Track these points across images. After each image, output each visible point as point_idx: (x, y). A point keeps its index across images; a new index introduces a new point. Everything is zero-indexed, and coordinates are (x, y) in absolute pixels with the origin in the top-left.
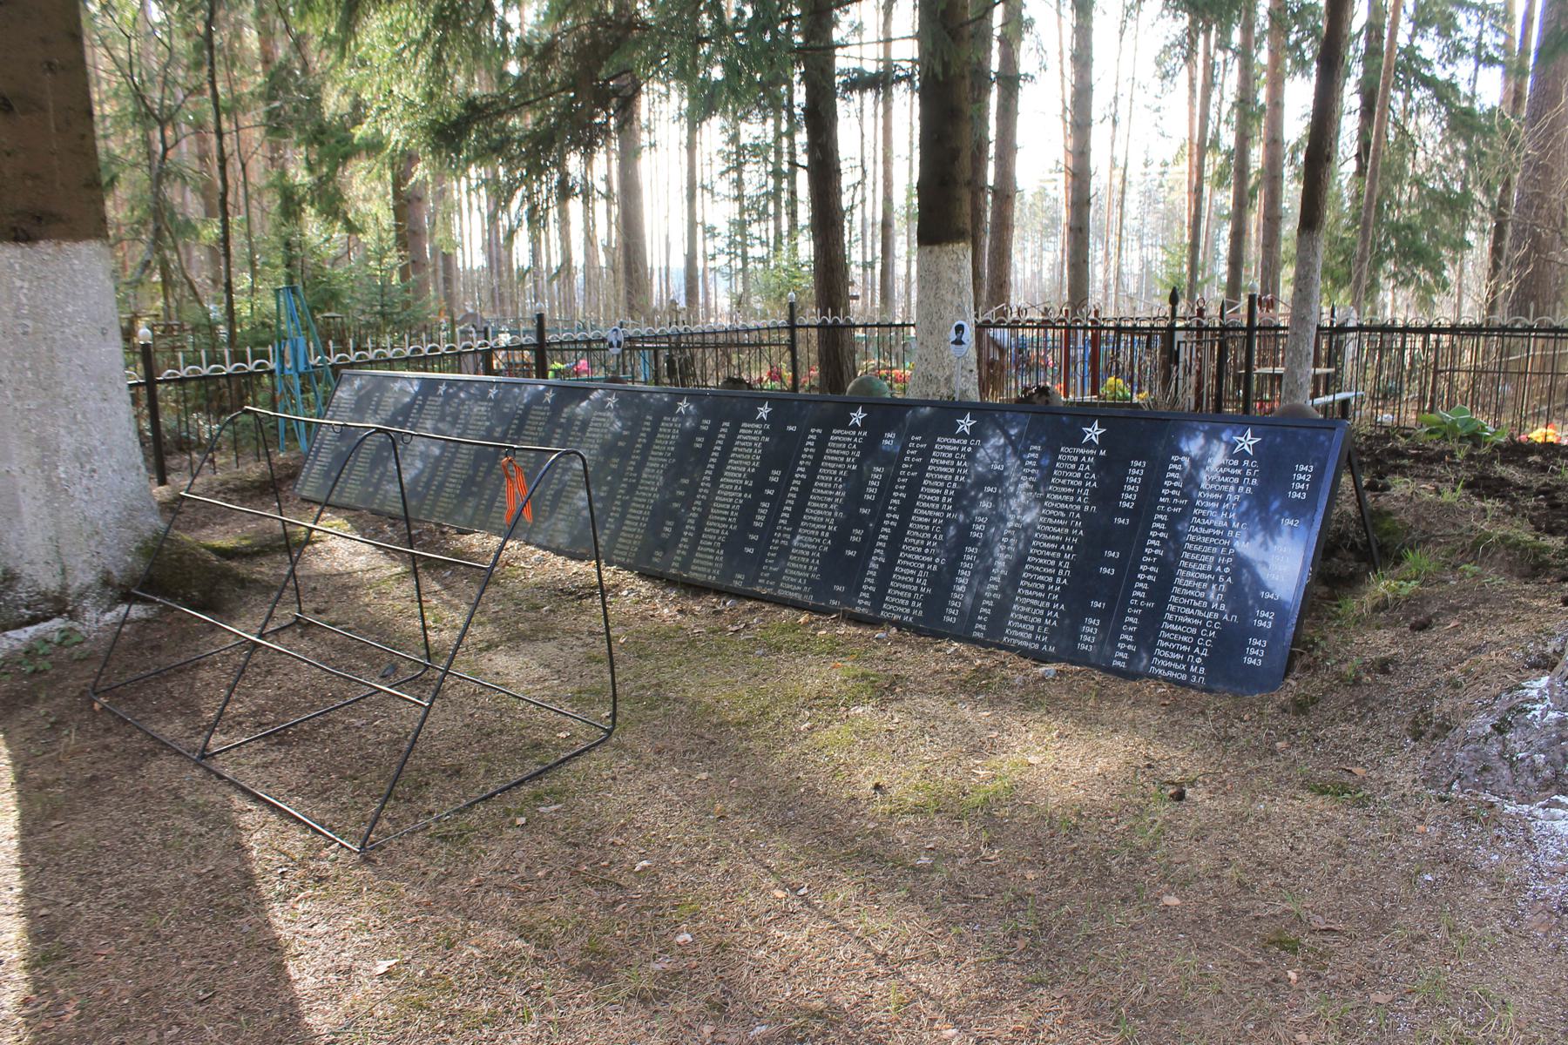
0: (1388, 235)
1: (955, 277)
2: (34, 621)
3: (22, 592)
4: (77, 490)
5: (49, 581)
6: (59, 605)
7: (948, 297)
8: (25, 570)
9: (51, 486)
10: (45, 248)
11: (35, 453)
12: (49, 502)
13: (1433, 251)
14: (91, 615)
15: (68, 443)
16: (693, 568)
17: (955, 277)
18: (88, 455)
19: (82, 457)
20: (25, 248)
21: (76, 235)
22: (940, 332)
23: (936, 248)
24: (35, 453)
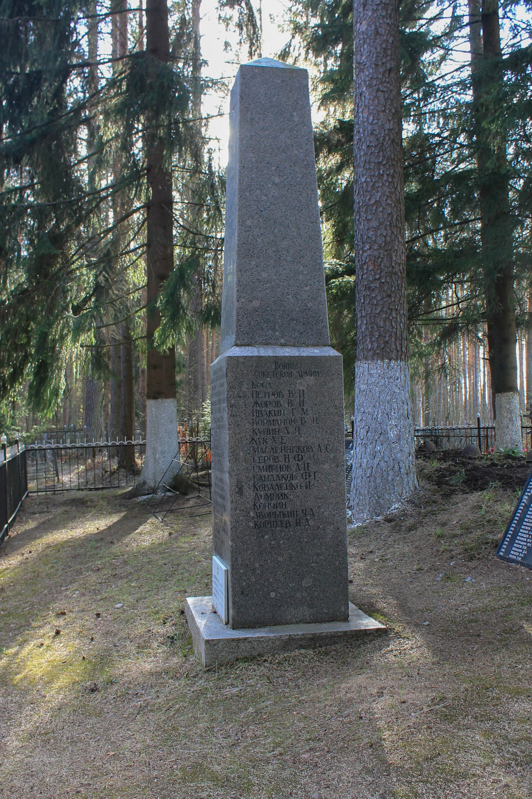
0: (124, 78)
1: (508, 406)
2: (148, 494)
3: (146, 487)
4: (160, 461)
5: (152, 484)
6: (154, 491)
7: (505, 414)
8: (148, 481)
9: (155, 460)
10: (160, 400)
11: (152, 451)
12: (154, 464)
13: (84, 43)
14: (159, 493)
15: (159, 449)
16: (512, 552)
17: (508, 406)
18: (164, 452)
19: (163, 453)
20: (155, 400)
21: (167, 397)
22: (502, 429)
23: (500, 394)
24: (152, 451)
